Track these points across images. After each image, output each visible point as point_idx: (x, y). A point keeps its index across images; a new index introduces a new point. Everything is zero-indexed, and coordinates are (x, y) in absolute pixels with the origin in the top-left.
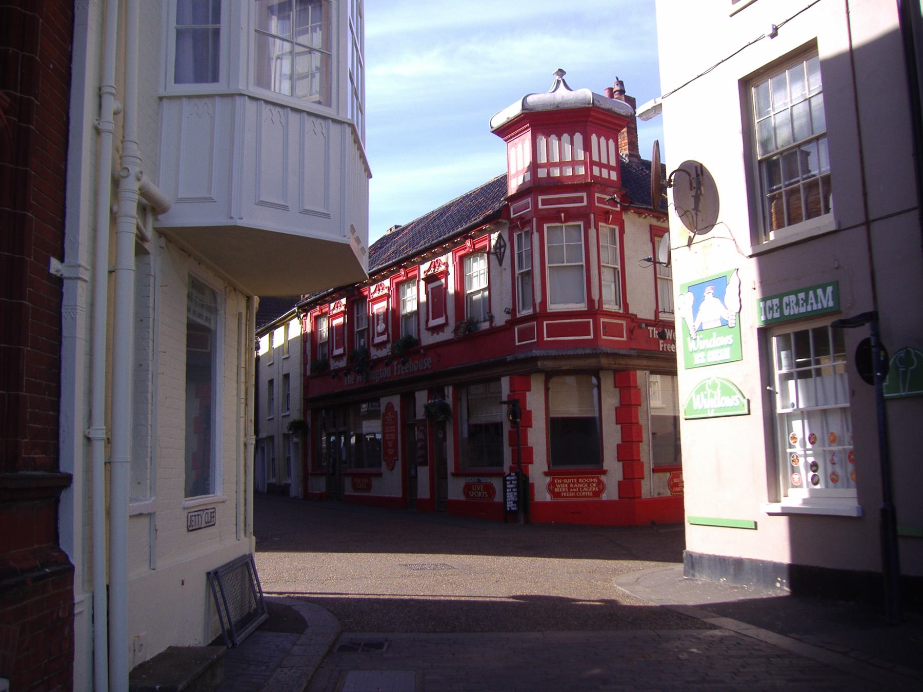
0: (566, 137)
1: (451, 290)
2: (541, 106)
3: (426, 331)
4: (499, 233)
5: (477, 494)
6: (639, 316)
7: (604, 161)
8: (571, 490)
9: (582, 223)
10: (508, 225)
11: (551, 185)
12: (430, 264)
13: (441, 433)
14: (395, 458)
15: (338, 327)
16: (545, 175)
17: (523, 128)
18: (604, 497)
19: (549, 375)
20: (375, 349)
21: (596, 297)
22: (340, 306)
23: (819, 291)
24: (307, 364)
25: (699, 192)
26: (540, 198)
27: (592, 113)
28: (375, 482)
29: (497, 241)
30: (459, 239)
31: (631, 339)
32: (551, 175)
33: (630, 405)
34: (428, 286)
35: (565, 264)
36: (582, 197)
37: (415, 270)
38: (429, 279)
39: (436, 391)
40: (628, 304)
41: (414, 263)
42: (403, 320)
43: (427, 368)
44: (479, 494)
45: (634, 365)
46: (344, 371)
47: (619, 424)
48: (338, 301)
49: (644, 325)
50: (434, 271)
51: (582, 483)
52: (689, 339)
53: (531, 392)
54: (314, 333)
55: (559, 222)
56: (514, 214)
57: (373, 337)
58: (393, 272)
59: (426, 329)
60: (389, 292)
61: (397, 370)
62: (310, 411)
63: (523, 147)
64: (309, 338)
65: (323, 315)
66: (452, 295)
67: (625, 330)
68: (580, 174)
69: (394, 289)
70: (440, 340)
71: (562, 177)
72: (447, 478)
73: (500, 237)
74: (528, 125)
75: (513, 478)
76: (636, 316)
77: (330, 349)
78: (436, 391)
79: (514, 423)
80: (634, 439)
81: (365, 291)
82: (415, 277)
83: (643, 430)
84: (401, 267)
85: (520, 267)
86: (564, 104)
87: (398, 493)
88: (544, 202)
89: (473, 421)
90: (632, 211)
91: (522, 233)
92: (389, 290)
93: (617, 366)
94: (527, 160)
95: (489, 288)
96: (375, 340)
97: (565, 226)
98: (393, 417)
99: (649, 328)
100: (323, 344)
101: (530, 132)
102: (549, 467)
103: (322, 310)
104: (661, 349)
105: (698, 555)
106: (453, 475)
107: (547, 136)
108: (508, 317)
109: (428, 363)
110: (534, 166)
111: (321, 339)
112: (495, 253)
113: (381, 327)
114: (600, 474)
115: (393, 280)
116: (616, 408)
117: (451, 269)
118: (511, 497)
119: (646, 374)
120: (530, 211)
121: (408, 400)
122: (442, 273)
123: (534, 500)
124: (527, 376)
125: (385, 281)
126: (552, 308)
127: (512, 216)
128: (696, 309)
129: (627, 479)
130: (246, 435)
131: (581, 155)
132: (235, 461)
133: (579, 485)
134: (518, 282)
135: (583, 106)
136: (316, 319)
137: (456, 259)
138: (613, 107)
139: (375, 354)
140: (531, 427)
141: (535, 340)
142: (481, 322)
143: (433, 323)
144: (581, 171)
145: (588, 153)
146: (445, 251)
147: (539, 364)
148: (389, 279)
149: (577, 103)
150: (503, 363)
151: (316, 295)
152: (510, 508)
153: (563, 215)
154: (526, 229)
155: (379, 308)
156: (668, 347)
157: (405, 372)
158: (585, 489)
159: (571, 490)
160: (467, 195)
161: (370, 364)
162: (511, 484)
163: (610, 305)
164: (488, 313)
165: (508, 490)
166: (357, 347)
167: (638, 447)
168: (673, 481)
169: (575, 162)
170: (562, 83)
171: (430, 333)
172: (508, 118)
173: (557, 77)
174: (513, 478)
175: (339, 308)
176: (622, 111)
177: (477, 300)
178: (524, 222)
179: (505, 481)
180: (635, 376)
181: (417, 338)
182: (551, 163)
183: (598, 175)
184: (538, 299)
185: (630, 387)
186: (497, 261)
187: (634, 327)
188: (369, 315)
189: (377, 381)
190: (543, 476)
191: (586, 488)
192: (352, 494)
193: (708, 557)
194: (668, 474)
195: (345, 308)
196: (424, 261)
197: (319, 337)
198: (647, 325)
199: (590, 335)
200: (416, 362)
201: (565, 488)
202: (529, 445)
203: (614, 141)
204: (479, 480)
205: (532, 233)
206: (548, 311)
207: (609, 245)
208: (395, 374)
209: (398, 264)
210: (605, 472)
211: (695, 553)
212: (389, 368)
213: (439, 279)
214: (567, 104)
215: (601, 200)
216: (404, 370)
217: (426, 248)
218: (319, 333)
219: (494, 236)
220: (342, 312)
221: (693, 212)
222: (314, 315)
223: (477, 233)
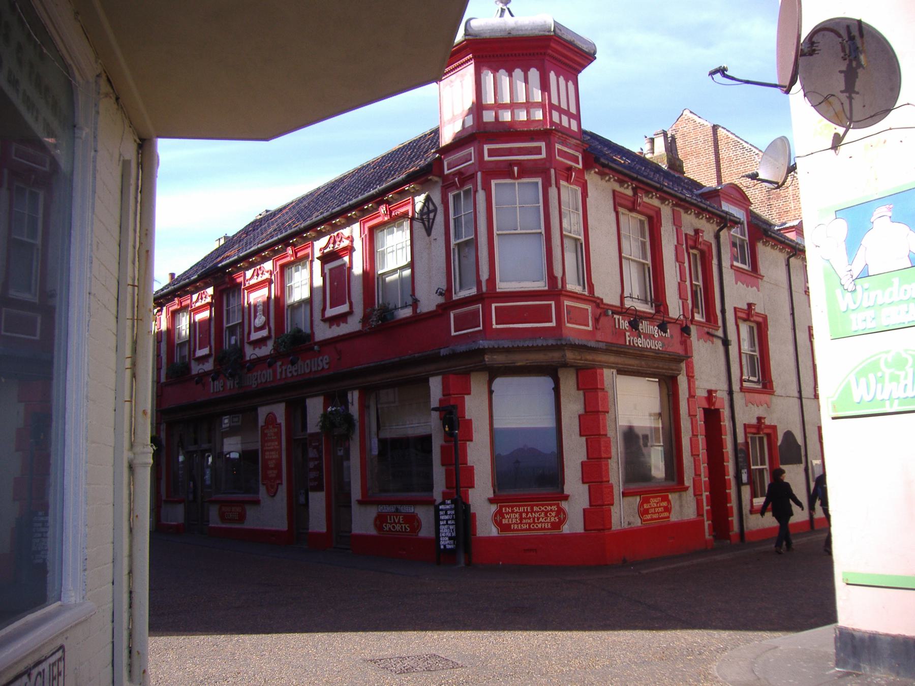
0: (518, 73)
1: (358, 269)
2: (489, 31)
3: (322, 323)
4: (426, 194)
5: (394, 527)
6: (605, 301)
7: (564, 106)
8: (524, 521)
9: (539, 180)
10: (440, 184)
11: (502, 131)
12: (328, 239)
13: (340, 450)
14: (279, 482)
15: (202, 322)
16: (493, 120)
17: (464, 60)
18: (566, 529)
19: (494, 372)
20: (252, 348)
21: (558, 273)
22: (205, 297)
24: (161, 368)
25: (854, 64)
26: (486, 147)
27: (552, 45)
28: (250, 512)
29: (424, 204)
30: (370, 205)
31: (596, 328)
32: (501, 120)
33: (598, 412)
34: (325, 266)
35: (519, 231)
36: (540, 148)
37: (307, 248)
38: (326, 258)
39: (336, 397)
40: (593, 285)
41: (306, 239)
42: (289, 312)
43: (323, 368)
44: (398, 527)
45: (600, 362)
46: (212, 375)
47: (583, 436)
48: (202, 292)
49: (610, 313)
50: (333, 247)
51: (538, 512)
52: (839, 290)
54: (171, 332)
55: (511, 178)
56: (448, 170)
57: (249, 333)
58: (278, 252)
60: (271, 277)
61: (281, 373)
62: (165, 425)
63: (462, 85)
64: (164, 338)
65: (183, 309)
66: (359, 276)
67: (590, 318)
68: (537, 119)
69: (277, 273)
70: (341, 334)
71: (513, 122)
72: (350, 507)
73: (428, 200)
74: (471, 56)
75: (448, 507)
76: (602, 300)
77: (192, 350)
78: (336, 397)
79: (449, 436)
80: (604, 455)
81: (239, 277)
82: (307, 256)
83: (612, 444)
84: (288, 245)
85: (457, 236)
86: (518, 30)
87: (282, 525)
88: (492, 153)
89: (387, 434)
90: (597, 170)
92: (271, 275)
93: (583, 362)
94: (469, 98)
95: (412, 265)
96: (251, 336)
97: (518, 183)
98: (276, 430)
99: (615, 316)
100: (182, 345)
101: (473, 64)
102: (494, 492)
103: (181, 303)
104: (628, 343)
105: (867, 635)
106: (360, 502)
107: (495, 70)
108: (441, 300)
109: (325, 362)
110: (478, 108)
111: (179, 338)
112: (422, 220)
113: (260, 320)
114: (561, 500)
115: (364, 223)
116: (580, 416)
117: (358, 245)
118: (446, 531)
119: (613, 373)
120: (473, 163)
121: (297, 410)
122: (345, 249)
123: (476, 535)
124: (467, 374)
125: (265, 264)
126: (502, 286)
127: (446, 172)
128: (853, 244)
129: (593, 506)
130: (132, 446)
131: (537, 96)
132: (110, 508)
133: (533, 514)
134: (454, 255)
135: (542, 33)
136: (174, 315)
137: (364, 231)
138: (575, 40)
139: (251, 353)
140: (471, 440)
141: (481, 328)
142: (399, 308)
143: (331, 312)
144: (538, 115)
145: (546, 93)
146: (350, 222)
148: (272, 261)
149: (535, 29)
150: (436, 358)
151: (174, 285)
152: (445, 546)
153: (516, 169)
155: (257, 297)
156: (635, 341)
157: (293, 375)
158: (543, 520)
159: (524, 521)
160: (363, 167)
161: (248, 365)
162: (446, 514)
163: (573, 286)
164: (411, 296)
165: (441, 523)
166: (226, 346)
167: (607, 465)
168: (643, 507)
169: (530, 104)
170: (507, 11)
171: (327, 325)
173: (501, 5)
174: (448, 507)
175: (204, 299)
176: (585, 46)
177: (392, 282)
178: (465, 177)
179: (437, 511)
180: (602, 375)
181: (309, 331)
182: (501, 104)
183: (558, 122)
184: (485, 276)
185: (597, 388)
186: (424, 230)
187: (601, 314)
188: (243, 306)
189: (254, 386)
190: (487, 504)
191: (543, 518)
192: (219, 526)
193: (889, 639)
194: (638, 498)
195: (212, 299)
196: (321, 235)
197: (176, 336)
198: (613, 313)
199: (551, 321)
200: (308, 361)
201: (516, 518)
202: (470, 463)
203: (574, 84)
204: (397, 509)
205: (476, 191)
206: (498, 290)
207: (571, 210)
208: (278, 377)
209: (285, 242)
210: (566, 498)
211: (859, 631)
212: (270, 371)
213: (341, 257)
214: (522, 30)
215: (562, 154)
216: (290, 372)
217: (324, 218)
218: (177, 332)
219: (420, 200)
220: (208, 304)
221: (844, 97)
222: (171, 309)
223: (396, 197)
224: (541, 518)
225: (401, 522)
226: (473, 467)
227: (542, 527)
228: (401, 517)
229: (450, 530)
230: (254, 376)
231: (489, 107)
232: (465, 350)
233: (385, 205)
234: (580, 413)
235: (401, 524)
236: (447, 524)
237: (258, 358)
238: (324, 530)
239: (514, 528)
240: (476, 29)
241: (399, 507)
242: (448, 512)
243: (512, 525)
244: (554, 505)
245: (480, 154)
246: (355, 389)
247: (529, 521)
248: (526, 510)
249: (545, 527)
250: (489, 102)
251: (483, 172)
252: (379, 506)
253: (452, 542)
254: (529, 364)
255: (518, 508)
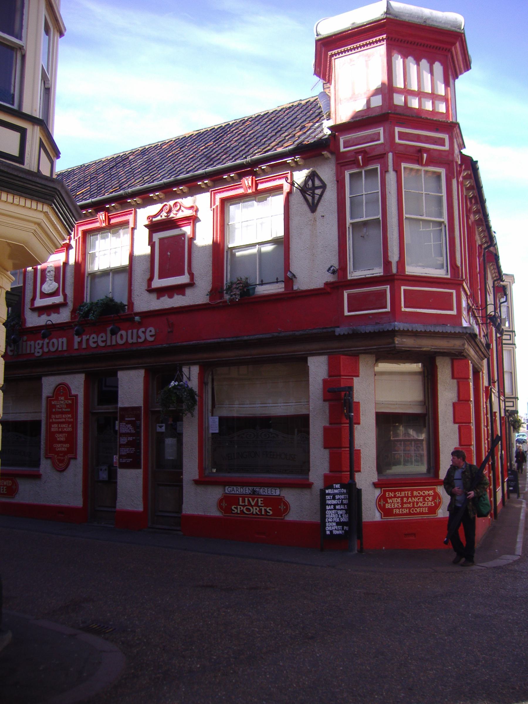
2: (407, 15)
13: (161, 427)
23: (60, 349)
26: (397, 129)
42: (89, 279)
51: (417, 496)
53: (359, 378)
55: (419, 164)
59: (31, 309)
66: (204, 248)
73: (312, 176)
74: (384, 36)
75: (336, 491)
91: (360, 173)
106: (197, 482)
107: (405, 56)
108: (330, 278)
115: (214, 194)
126: (411, 270)
133: (413, 498)
134: (349, 234)
140: (359, 424)
143: (157, 283)
147: (398, 341)
149: (447, 23)
152: (331, 532)
153: (425, 155)
154: (370, 167)
158: (420, 504)
159: (405, 506)
162: (334, 498)
165: (328, 507)
169: (435, 96)
172: (353, 24)
174: (336, 491)
190: (371, 488)
191: (421, 502)
201: (398, 503)
204: (254, 492)
214: (436, 21)
223: (269, 169)
224: (420, 503)
225: (259, 504)
226: (359, 450)
227: (420, 511)
228: (259, 500)
229: (338, 515)
230: (39, 344)
231: (400, 91)
232: (372, 331)
233: (251, 177)
234: (454, 401)
235: (259, 506)
236: (335, 509)
237: (53, 325)
238: (141, 509)
239: (396, 512)
240: (396, 10)
241: (257, 489)
242: (336, 496)
243: (394, 510)
244: (431, 489)
245: (390, 136)
246: (194, 364)
247: (409, 506)
248: (406, 495)
249: (422, 511)
250: (398, 86)
251: (396, 153)
252: (227, 487)
253: (340, 527)
254: (433, 350)
255: (400, 493)
